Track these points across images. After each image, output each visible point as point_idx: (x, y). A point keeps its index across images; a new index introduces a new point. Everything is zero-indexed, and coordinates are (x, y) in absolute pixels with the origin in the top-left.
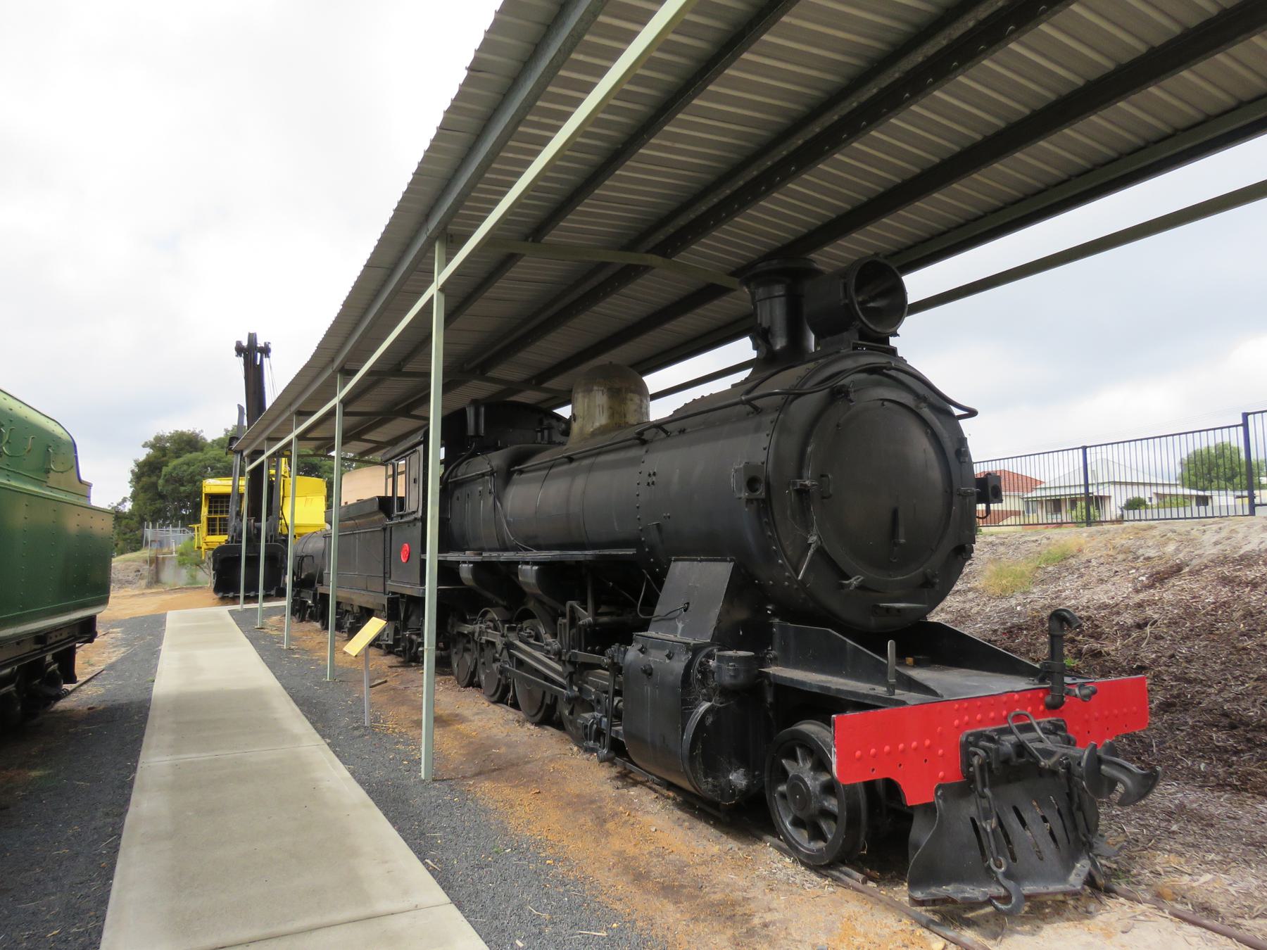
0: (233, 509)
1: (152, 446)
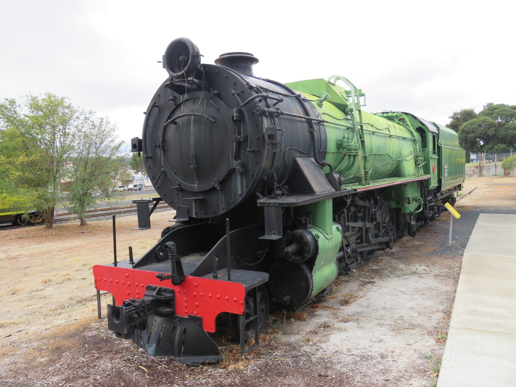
1: (453, 118)
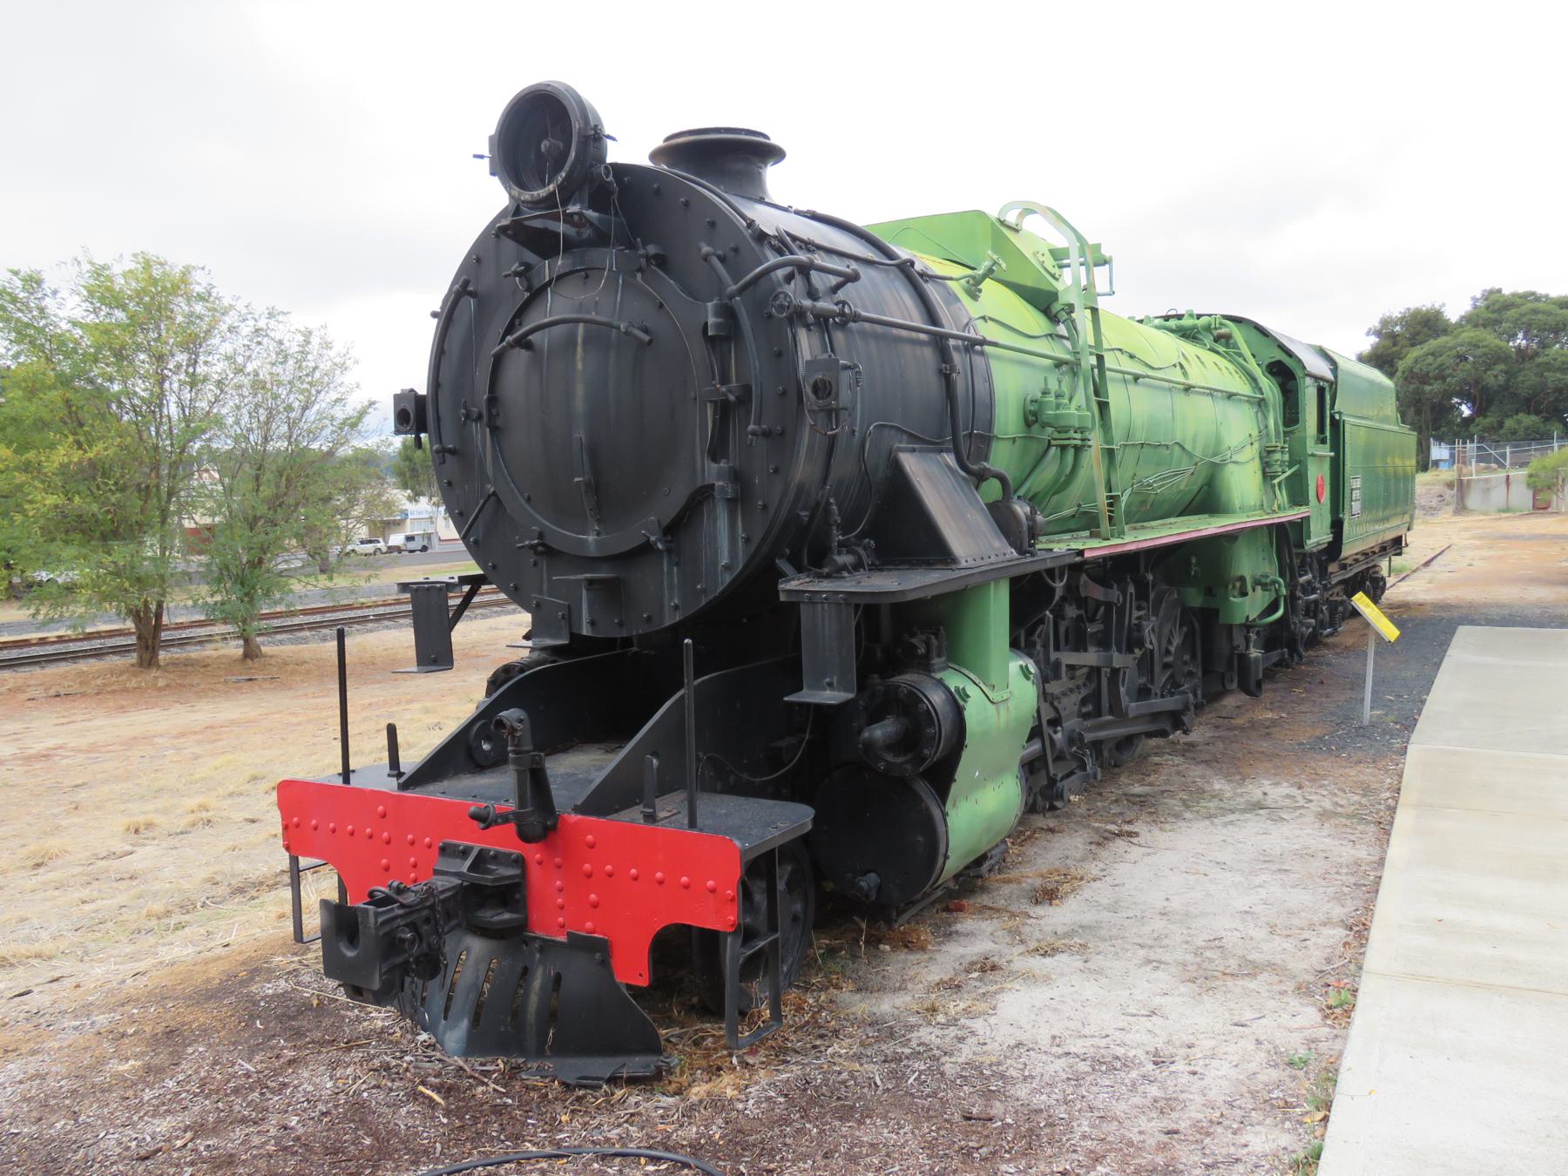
1: (1378, 333)
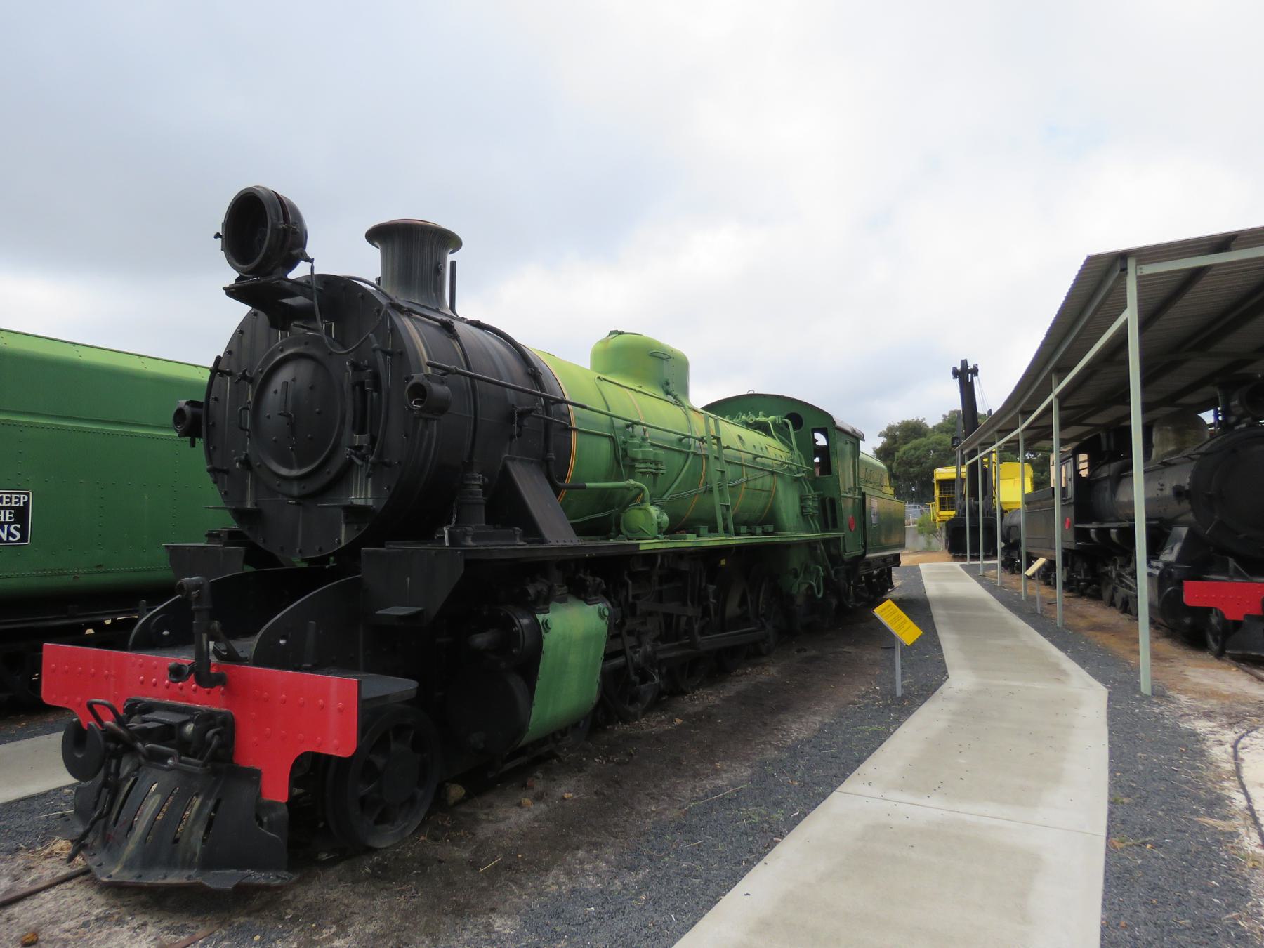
0: (958, 491)
1: (885, 435)
